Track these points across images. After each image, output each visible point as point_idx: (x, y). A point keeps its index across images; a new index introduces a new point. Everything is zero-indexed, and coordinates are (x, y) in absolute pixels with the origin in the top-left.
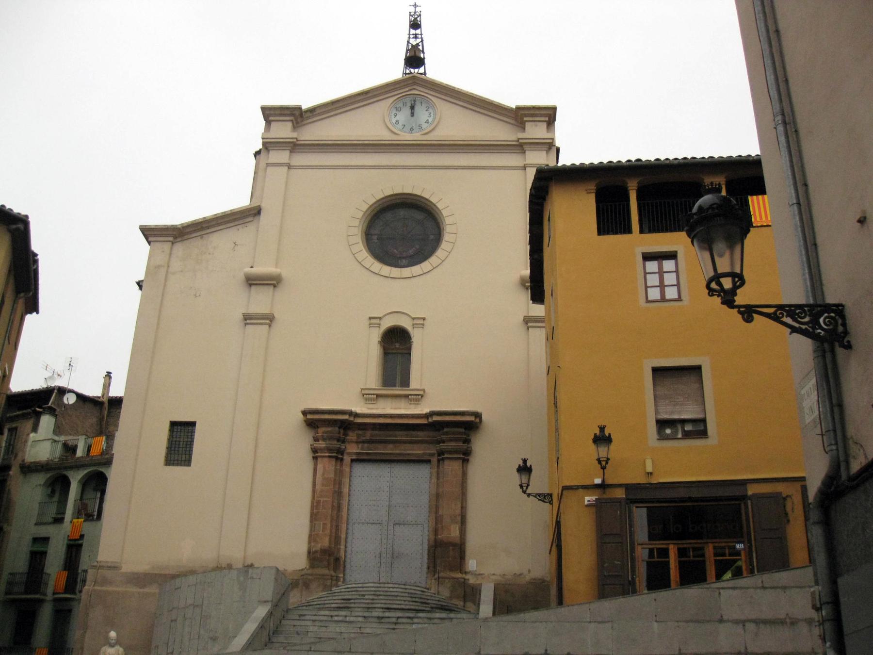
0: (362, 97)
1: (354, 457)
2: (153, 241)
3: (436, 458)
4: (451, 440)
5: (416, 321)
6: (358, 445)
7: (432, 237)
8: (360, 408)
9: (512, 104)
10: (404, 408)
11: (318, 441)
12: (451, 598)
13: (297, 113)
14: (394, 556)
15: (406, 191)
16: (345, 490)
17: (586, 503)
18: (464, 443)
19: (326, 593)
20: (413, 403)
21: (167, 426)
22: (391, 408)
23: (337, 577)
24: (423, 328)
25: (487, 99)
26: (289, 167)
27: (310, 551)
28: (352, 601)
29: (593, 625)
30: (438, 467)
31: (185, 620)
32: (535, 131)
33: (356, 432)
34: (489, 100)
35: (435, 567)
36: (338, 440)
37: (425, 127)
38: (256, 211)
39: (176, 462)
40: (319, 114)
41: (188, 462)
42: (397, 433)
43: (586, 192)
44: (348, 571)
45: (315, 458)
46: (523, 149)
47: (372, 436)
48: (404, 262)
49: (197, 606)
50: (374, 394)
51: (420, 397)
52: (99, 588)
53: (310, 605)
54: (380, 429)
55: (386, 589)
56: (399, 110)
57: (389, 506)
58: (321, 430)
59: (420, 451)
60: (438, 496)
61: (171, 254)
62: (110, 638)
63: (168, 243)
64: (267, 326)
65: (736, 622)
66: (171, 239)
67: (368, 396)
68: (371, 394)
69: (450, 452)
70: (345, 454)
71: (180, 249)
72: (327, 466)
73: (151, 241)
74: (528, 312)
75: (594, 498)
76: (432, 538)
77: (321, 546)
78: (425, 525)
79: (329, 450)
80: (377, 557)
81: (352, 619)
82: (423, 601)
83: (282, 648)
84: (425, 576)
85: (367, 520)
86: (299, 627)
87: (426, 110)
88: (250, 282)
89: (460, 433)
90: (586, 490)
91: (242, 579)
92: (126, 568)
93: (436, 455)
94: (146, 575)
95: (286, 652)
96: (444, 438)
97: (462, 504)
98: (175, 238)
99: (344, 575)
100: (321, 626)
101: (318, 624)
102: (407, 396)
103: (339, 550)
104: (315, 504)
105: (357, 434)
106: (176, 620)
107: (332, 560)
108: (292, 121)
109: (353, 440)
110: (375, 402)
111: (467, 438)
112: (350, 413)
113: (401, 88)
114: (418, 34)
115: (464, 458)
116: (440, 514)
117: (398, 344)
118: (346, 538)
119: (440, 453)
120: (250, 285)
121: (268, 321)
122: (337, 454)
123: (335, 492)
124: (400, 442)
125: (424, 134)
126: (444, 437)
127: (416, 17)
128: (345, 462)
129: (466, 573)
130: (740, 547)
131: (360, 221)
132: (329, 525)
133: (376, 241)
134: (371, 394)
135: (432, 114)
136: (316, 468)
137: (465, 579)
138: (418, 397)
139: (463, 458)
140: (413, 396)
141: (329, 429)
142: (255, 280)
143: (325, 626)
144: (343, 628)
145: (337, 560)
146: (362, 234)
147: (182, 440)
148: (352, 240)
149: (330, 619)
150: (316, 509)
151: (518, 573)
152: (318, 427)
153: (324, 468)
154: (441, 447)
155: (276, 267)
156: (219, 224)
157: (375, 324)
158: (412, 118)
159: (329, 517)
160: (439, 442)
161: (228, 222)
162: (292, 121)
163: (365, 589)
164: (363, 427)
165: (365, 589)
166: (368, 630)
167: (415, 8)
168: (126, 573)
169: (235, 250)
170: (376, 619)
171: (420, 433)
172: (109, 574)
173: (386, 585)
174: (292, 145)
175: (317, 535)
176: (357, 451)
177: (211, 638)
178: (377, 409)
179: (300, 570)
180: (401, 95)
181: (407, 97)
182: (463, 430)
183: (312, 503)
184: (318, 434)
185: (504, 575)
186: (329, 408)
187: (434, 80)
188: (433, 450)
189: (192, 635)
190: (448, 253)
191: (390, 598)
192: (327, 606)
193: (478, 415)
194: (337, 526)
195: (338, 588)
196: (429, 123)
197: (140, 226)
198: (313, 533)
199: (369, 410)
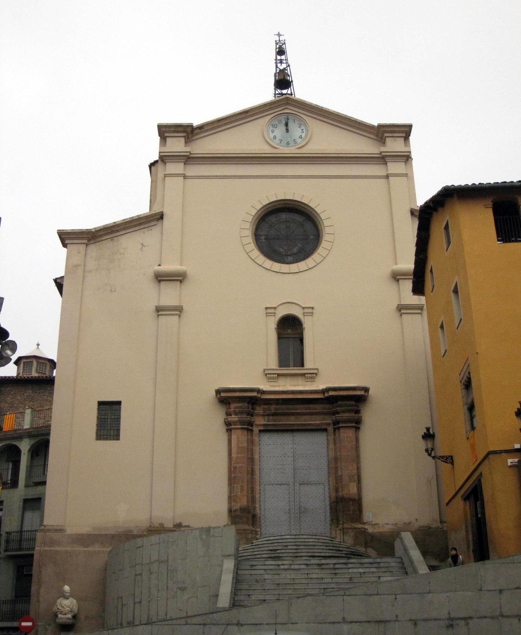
0: (243, 116)
1: (262, 428)
2: (69, 244)
3: (332, 427)
4: (344, 412)
6: (264, 418)
7: (312, 237)
8: (265, 386)
9: (375, 122)
10: (301, 385)
11: (231, 415)
12: (355, 545)
13: (189, 130)
14: (302, 511)
15: (288, 198)
16: (256, 456)
17: (509, 464)
18: (355, 413)
21: (96, 406)
22: (290, 386)
24: (312, 316)
25: (352, 117)
26: (185, 177)
27: (231, 510)
28: (278, 551)
31: (151, 573)
33: (262, 406)
34: (353, 118)
35: (338, 519)
36: (248, 415)
37: (299, 142)
38: (158, 217)
39: (106, 437)
40: (207, 131)
41: (116, 437)
42: (298, 406)
43: (484, 207)
45: (229, 431)
46: (385, 161)
47: (276, 409)
48: (290, 259)
49: (163, 562)
51: (315, 375)
52: (47, 548)
54: (283, 404)
55: (302, 540)
56: (276, 126)
57: (294, 469)
58: (233, 406)
61: (86, 255)
62: (64, 591)
63: (83, 245)
64: (177, 317)
66: (86, 241)
67: (270, 375)
68: (273, 374)
69: (345, 422)
70: (254, 426)
71: (93, 249)
72: (239, 436)
73: (67, 244)
74: (400, 301)
75: (516, 460)
76: (333, 495)
78: (325, 484)
79: (242, 423)
81: (296, 567)
82: (337, 549)
83: (322, 594)
84: (329, 527)
86: (255, 576)
87: (299, 127)
88: (159, 279)
89: (353, 406)
90: (508, 454)
91: (204, 537)
92: (69, 531)
93: (332, 424)
94: (89, 536)
95: (325, 597)
96: (339, 410)
97: (357, 465)
98: (89, 240)
100: (274, 574)
101: (269, 572)
102: (303, 375)
103: (255, 508)
106: (141, 574)
107: (250, 516)
108: (184, 136)
109: (260, 414)
110: (276, 381)
111: (358, 409)
112: (258, 391)
113: (276, 107)
114: (283, 60)
116: (339, 474)
120: (160, 281)
121: (178, 313)
122: (247, 426)
124: (299, 414)
125: (299, 148)
126: (338, 409)
127: (281, 45)
128: (254, 433)
129: (364, 523)
131: (250, 224)
132: (245, 488)
133: (264, 241)
134: (273, 374)
135: (304, 131)
137: (365, 529)
138: (313, 376)
139: (355, 426)
140: (308, 375)
141: (240, 405)
142: (163, 277)
143: (277, 574)
144: (290, 575)
145: (254, 516)
146: (252, 235)
147: (109, 418)
149: (277, 567)
151: (407, 522)
153: (238, 438)
154: (337, 418)
155: (181, 265)
156: (125, 229)
157: (271, 313)
158: (288, 133)
160: (334, 414)
161: (135, 226)
162: (184, 136)
163: (284, 541)
164: (268, 402)
165: (284, 541)
166: (314, 576)
167: (279, 37)
168: (72, 535)
169: (142, 251)
170: (317, 566)
172: (56, 536)
174: (186, 158)
175: (236, 495)
176: (264, 423)
177: (180, 589)
178: (279, 386)
180: (276, 114)
181: (282, 115)
182: (353, 403)
184: (230, 409)
185: (396, 524)
186: (240, 387)
187: (305, 101)
188: (329, 420)
189: (160, 586)
190: (329, 251)
193: (366, 390)
194: (252, 488)
195: (257, 541)
196: (302, 138)
197: (58, 230)
198: (233, 495)
199: (272, 387)
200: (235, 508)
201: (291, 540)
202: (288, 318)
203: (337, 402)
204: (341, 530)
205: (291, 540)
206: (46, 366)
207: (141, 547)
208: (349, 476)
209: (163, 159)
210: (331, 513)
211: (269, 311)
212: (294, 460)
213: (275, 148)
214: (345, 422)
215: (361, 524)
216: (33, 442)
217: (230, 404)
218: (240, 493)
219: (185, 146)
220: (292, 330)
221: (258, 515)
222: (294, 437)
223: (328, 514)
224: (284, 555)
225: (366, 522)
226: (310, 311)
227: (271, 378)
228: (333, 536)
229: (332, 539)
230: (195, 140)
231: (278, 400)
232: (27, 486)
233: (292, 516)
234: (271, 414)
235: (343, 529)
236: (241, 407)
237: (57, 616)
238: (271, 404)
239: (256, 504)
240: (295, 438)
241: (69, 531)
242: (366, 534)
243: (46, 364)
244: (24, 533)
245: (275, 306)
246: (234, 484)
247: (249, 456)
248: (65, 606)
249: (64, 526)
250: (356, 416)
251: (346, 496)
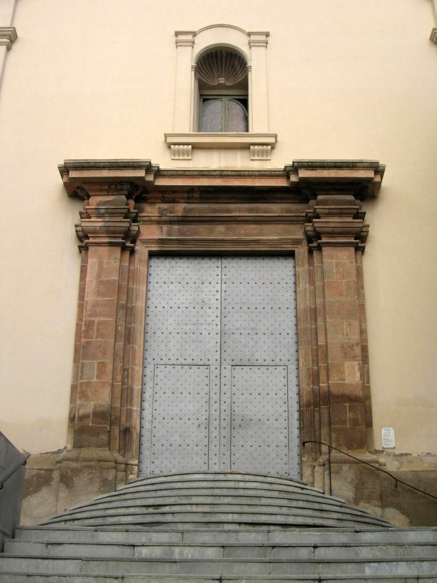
1: (155, 248)
5: (253, 38)
6: (161, 228)
11: (90, 218)
12: (356, 501)
19: (107, 495)
20: (256, 158)
23: (127, 464)
30: (311, 263)
33: (158, 205)
44: (146, 453)
50: (188, 144)
51: (269, 147)
53: (74, 520)
55: (231, 484)
57: (222, 333)
58: (95, 201)
59: (275, 236)
67: (177, 146)
68: (184, 144)
69: (331, 234)
70: (138, 243)
76: (306, 387)
77: (95, 406)
79: (110, 232)
80: (203, 426)
81: (189, 553)
84: (297, 460)
85: (182, 361)
93: (305, 242)
99: (140, 462)
102: (246, 147)
103: (129, 413)
104: (83, 328)
105: (159, 208)
107: (116, 432)
109: (153, 218)
110: (190, 158)
112: (148, 168)
115: (357, 243)
117: (223, 79)
118: (142, 392)
132: (110, 367)
134: (184, 144)
136: (86, 267)
140: (256, 147)
145: (127, 432)
150: (85, 337)
152: (89, 197)
153: (101, 263)
159: (110, 352)
160: (309, 220)
173: (230, 477)
175: (88, 384)
179: (54, 453)
183: (78, 326)
191: (243, 501)
192: (111, 520)
200: (82, 412)
201: (204, 484)
202: (219, 53)
204: (324, 465)
205: (204, 484)
208: (342, 347)
210: (301, 429)
211: (181, 38)
212: (222, 316)
214: (331, 234)
215: (370, 452)
218: (97, 377)
220: (227, 79)
221: (135, 429)
222: (224, 269)
223: (296, 432)
224: (178, 518)
225: (381, 449)
227: (178, 153)
228: (305, 480)
229: (302, 486)
231: (191, 189)
233: (213, 435)
234: (176, 219)
235: (330, 463)
238: (174, 201)
239: (131, 405)
240: (225, 271)
242: (382, 474)
245: (196, 29)
246: (83, 359)
250: (357, 223)
251: (334, 391)
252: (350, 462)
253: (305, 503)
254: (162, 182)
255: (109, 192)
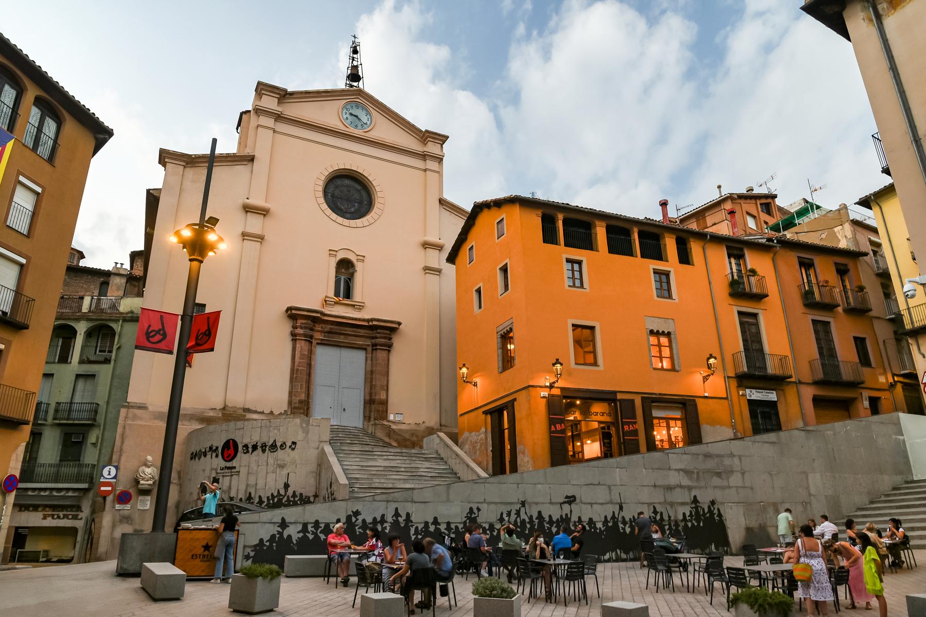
4: (381, 338)
5: (359, 257)
17: (542, 396)
26: (274, 131)
29: (618, 470)
32: (432, 148)
45: (294, 340)
48: (348, 215)
54: (337, 325)
58: (299, 322)
60: (372, 372)
65: (676, 470)
69: (381, 345)
72: (302, 345)
76: (368, 398)
79: (305, 335)
91: (304, 425)
98: (187, 164)
119: (374, 345)
120: (247, 212)
123: (308, 363)
128: (313, 345)
130: (629, 428)
132: (304, 386)
138: (359, 307)
141: (305, 321)
148: (379, 212)
153: (301, 347)
155: (266, 203)
160: (373, 338)
164: (327, 322)
171: (362, 331)
174: (277, 116)
182: (389, 332)
188: (368, 342)
193: (399, 324)
203: (377, 330)
206: (74, 257)
207: (237, 429)
209: (258, 111)
211: (332, 252)
213: (347, 127)
214: (381, 345)
216: (91, 324)
217: (297, 319)
219: (278, 106)
226: (362, 258)
230: (284, 103)
232: (81, 362)
236: (305, 323)
237: (139, 482)
241: (151, 408)
243: (74, 254)
244: (73, 404)
247: (309, 362)
248: (147, 474)
249: (146, 404)
252: (381, 425)
253: (344, 606)
254: (326, 318)
255: (304, 319)
